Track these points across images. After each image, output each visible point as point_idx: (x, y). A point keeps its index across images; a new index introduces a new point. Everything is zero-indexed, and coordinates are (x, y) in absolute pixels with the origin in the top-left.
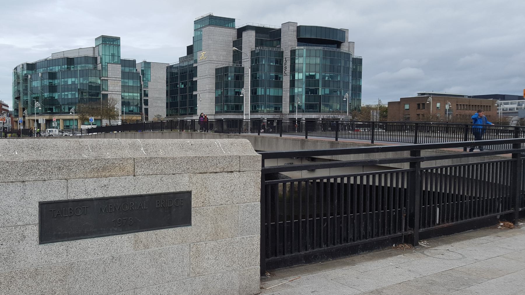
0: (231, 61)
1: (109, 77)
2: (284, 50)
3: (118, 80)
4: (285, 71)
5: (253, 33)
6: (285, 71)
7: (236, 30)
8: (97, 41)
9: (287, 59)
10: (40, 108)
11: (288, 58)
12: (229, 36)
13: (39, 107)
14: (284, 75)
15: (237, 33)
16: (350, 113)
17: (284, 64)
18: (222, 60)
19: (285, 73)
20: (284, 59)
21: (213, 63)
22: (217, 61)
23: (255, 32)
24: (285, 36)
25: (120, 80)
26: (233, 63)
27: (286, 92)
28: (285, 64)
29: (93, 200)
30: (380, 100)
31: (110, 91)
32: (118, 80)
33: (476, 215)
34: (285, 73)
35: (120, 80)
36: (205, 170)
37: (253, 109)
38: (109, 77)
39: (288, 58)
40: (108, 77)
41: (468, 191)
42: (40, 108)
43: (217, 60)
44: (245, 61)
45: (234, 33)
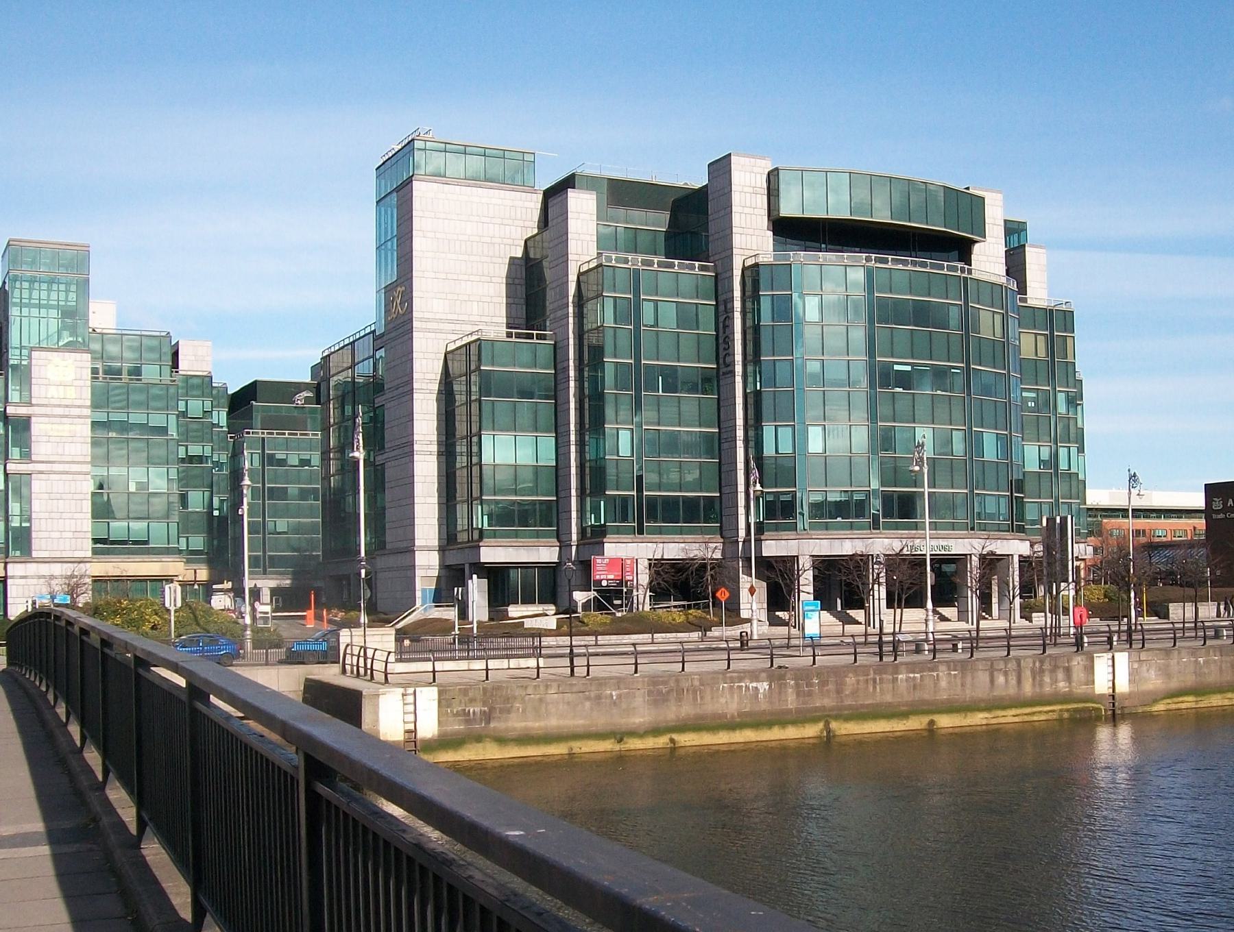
0: (421, 334)
1: (38, 405)
3: (79, 417)
4: (724, 358)
6: (724, 358)
8: (383, 209)
12: (510, 222)
14: (724, 374)
18: (477, 318)
21: (434, 331)
22: (451, 322)
23: (595, 196)
25: (86, 417)
26: (508, 327)
29: (507, 826)
30: (1135, 475)
31: (43, 462)
32: (79, 417)
35: (86, 417)
36: (41, 927)
38: (38, 405)
40: (30, 404)
43: (455, 317)
45: (534, 203)
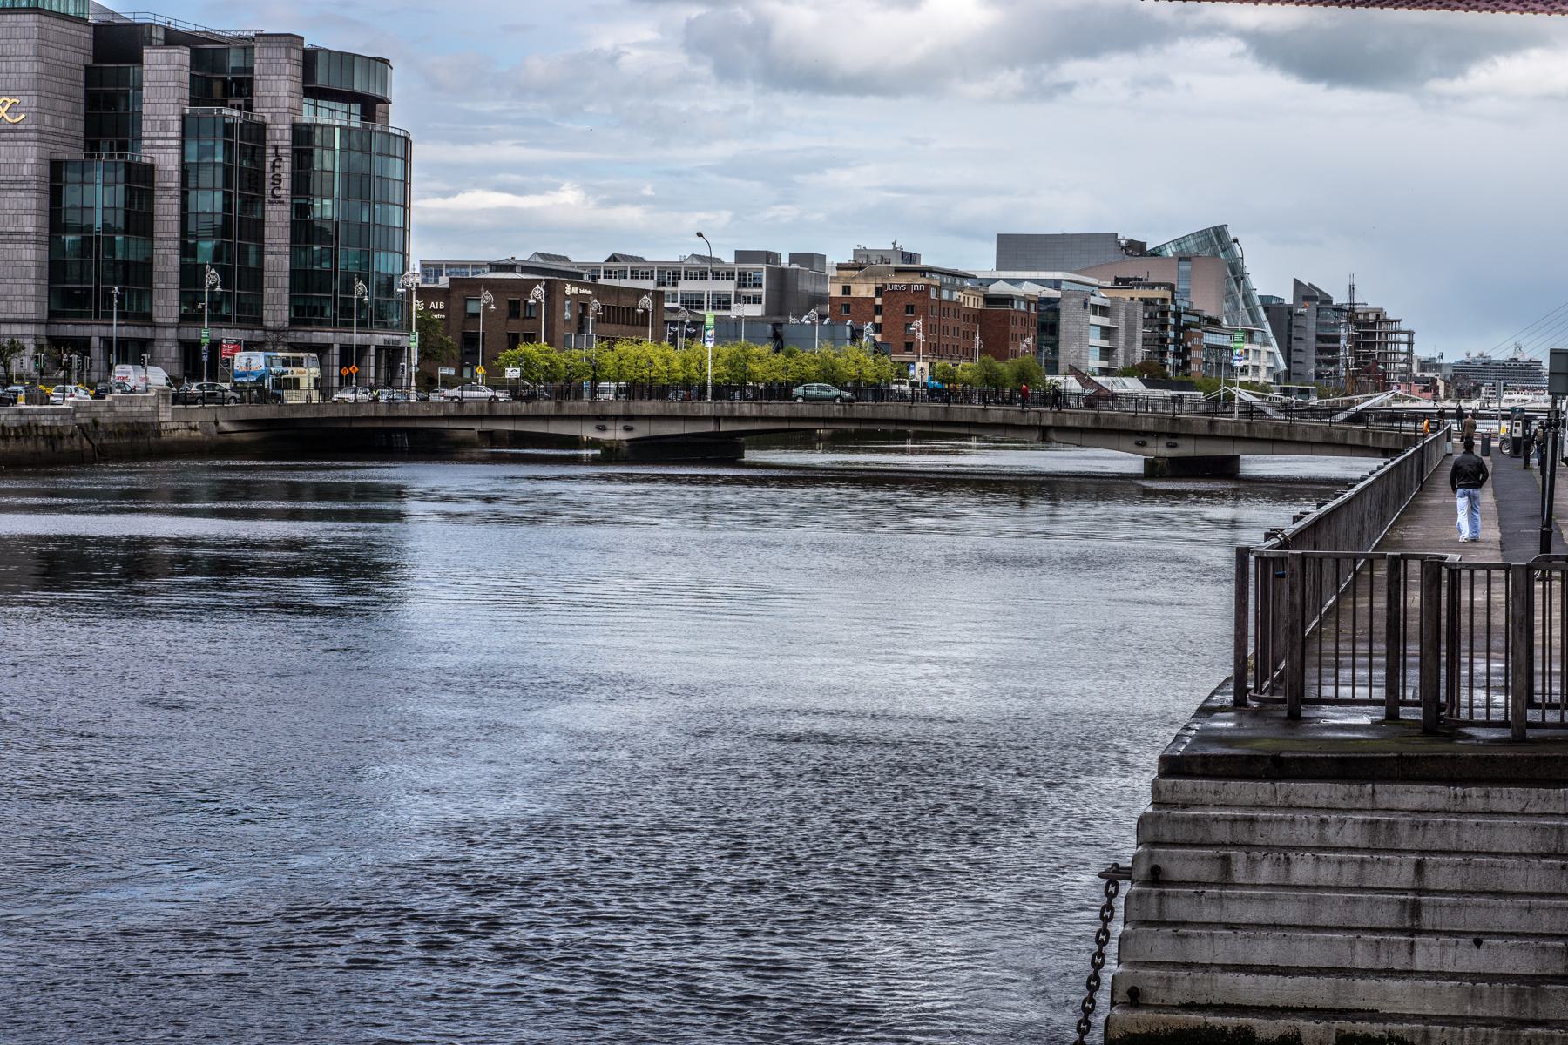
2: (268, 119)
5: (182, 55)
7: (88, 34)
9: (280, 151)
10: (493, 307)
11: (283, 147)
13: (490, 304)
14: (270, 202)
15: (94, 40)
16: (682, 302)
17: (268, 166)
19: (273, 195)
20: (270, 151)
24: (272, 77)
27: (279, 257)
28: (273, 167)
33: (1336, 345)
34: (273, 195)
37: (88, 315)
39: (283, 147)
41: (621, 479)
42: (493, 307)
44: (158, 147)
